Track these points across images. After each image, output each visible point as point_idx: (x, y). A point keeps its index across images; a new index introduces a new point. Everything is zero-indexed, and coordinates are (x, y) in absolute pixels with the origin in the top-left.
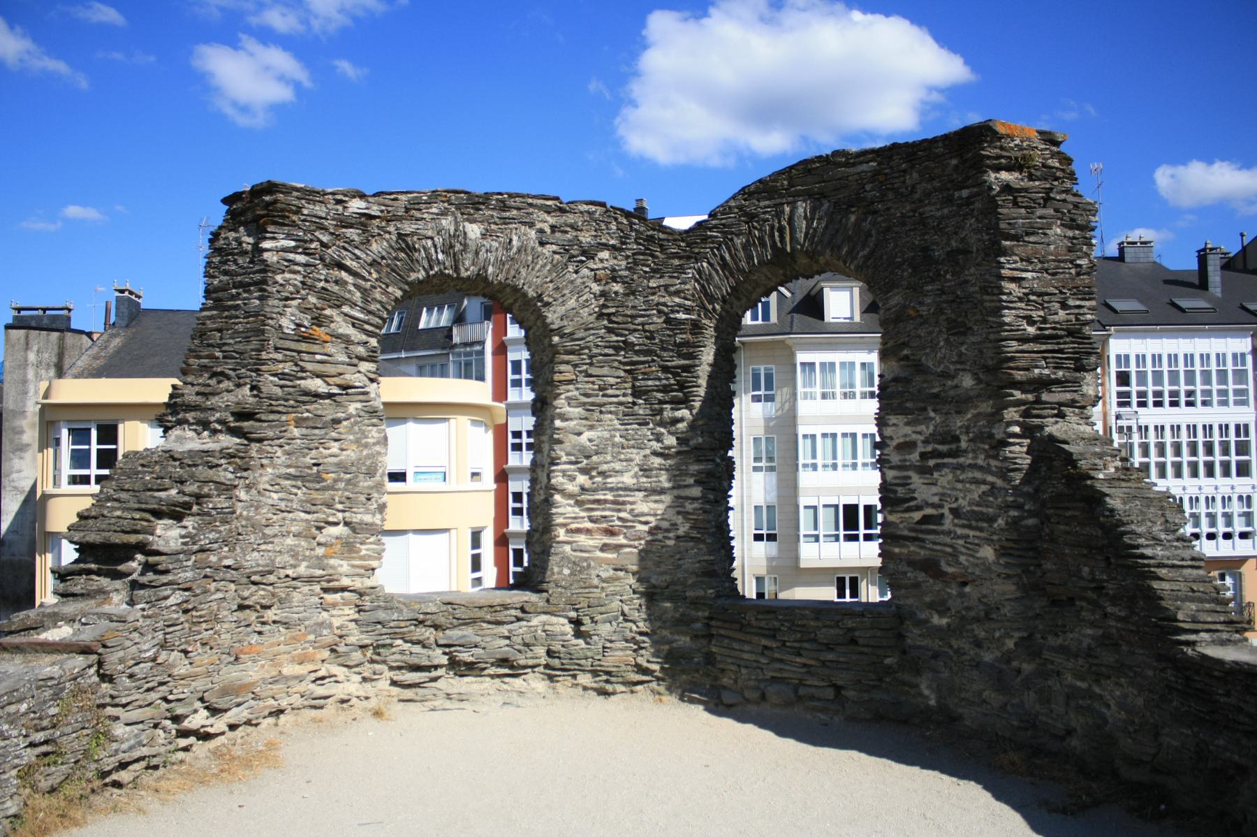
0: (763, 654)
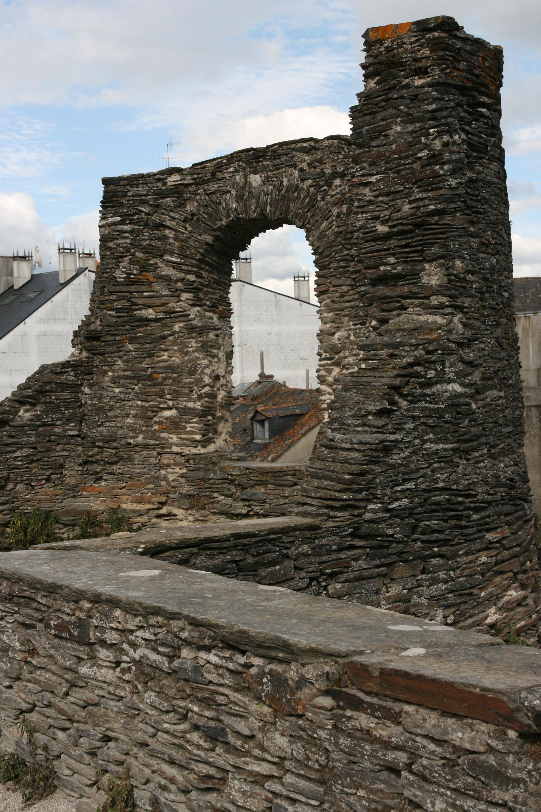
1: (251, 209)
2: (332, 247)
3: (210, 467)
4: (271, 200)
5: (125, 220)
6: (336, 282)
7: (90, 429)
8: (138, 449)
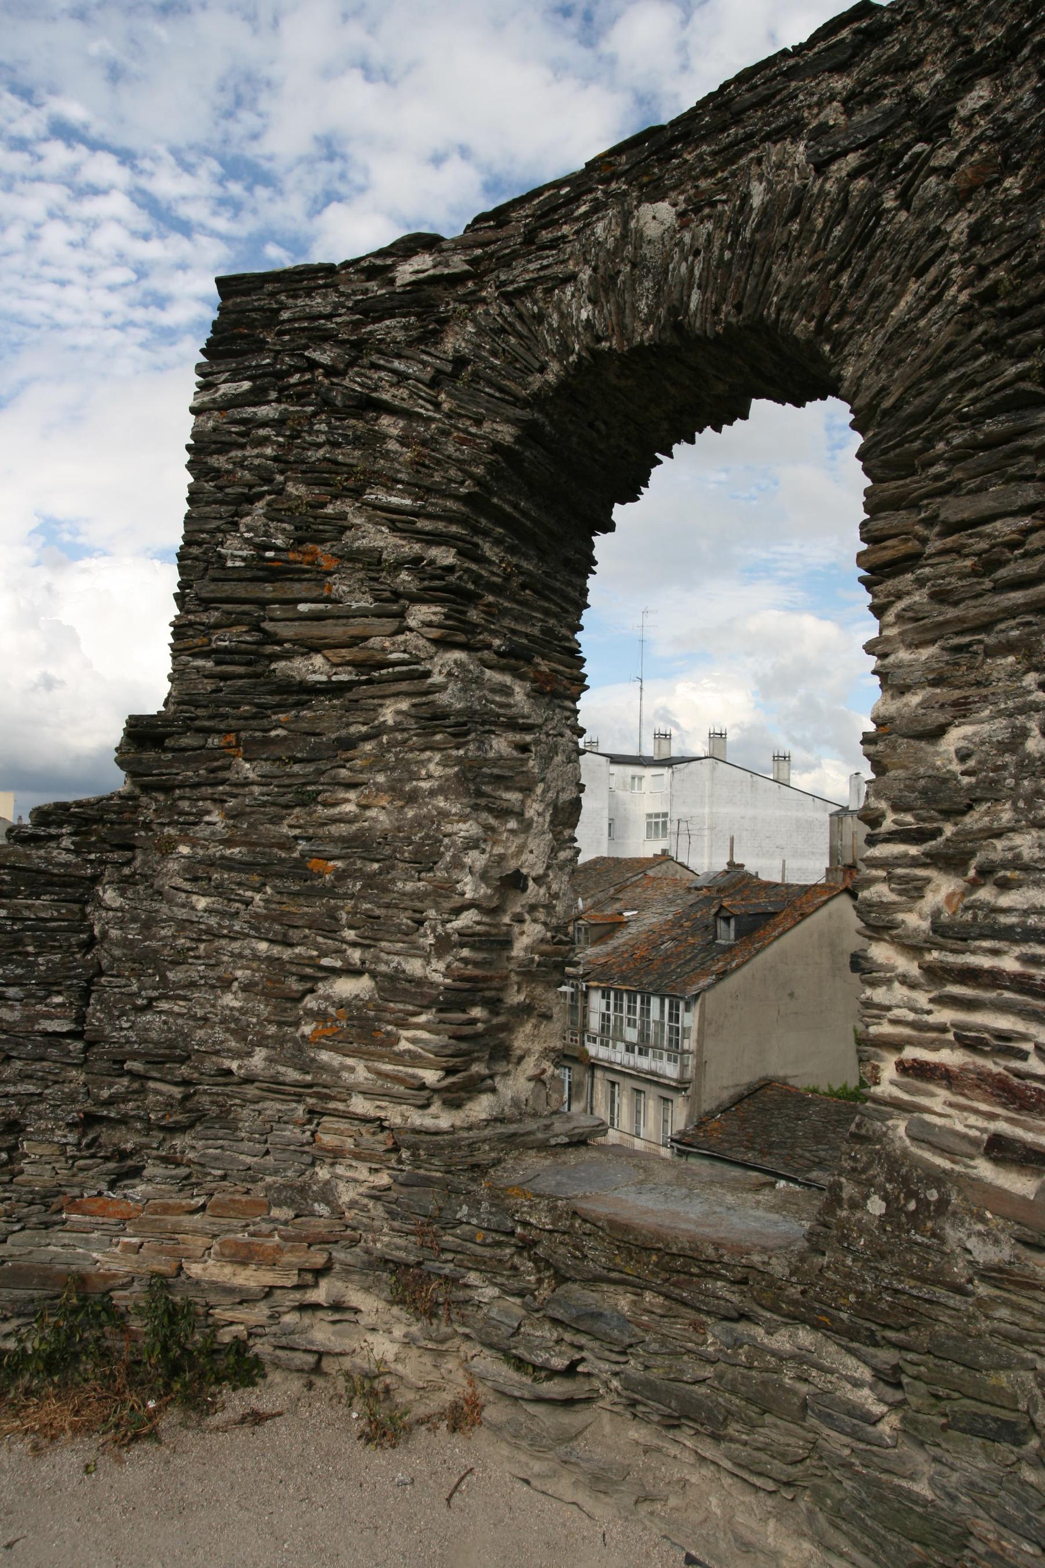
2: (945, 369)
3: (462, 1180)
4: (706, 269)
6: (954, 509)
7: (111, 1017)
8: (251, 1091)
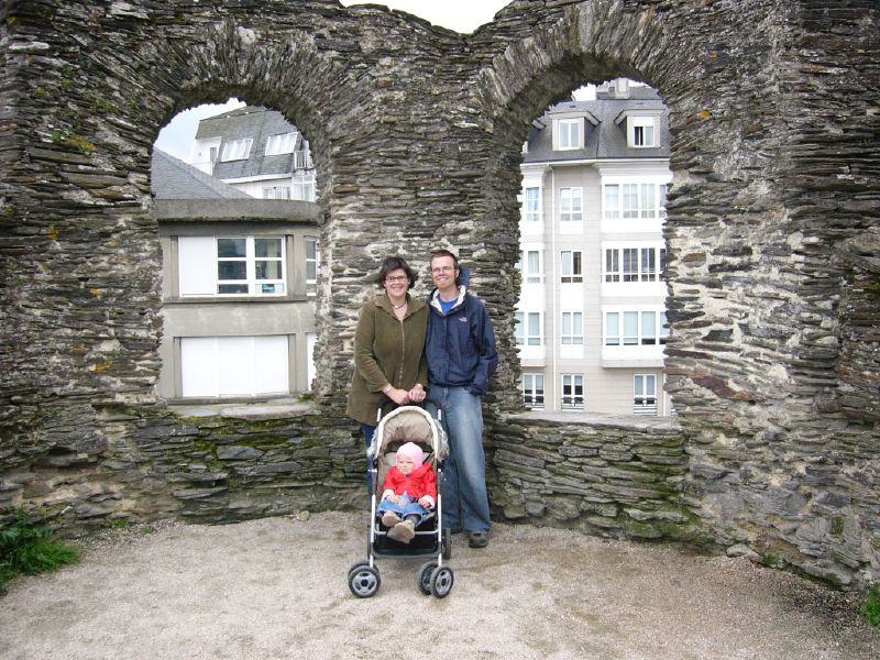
0: (545, 468)
1: (239, 72)
5: (54, 51)
